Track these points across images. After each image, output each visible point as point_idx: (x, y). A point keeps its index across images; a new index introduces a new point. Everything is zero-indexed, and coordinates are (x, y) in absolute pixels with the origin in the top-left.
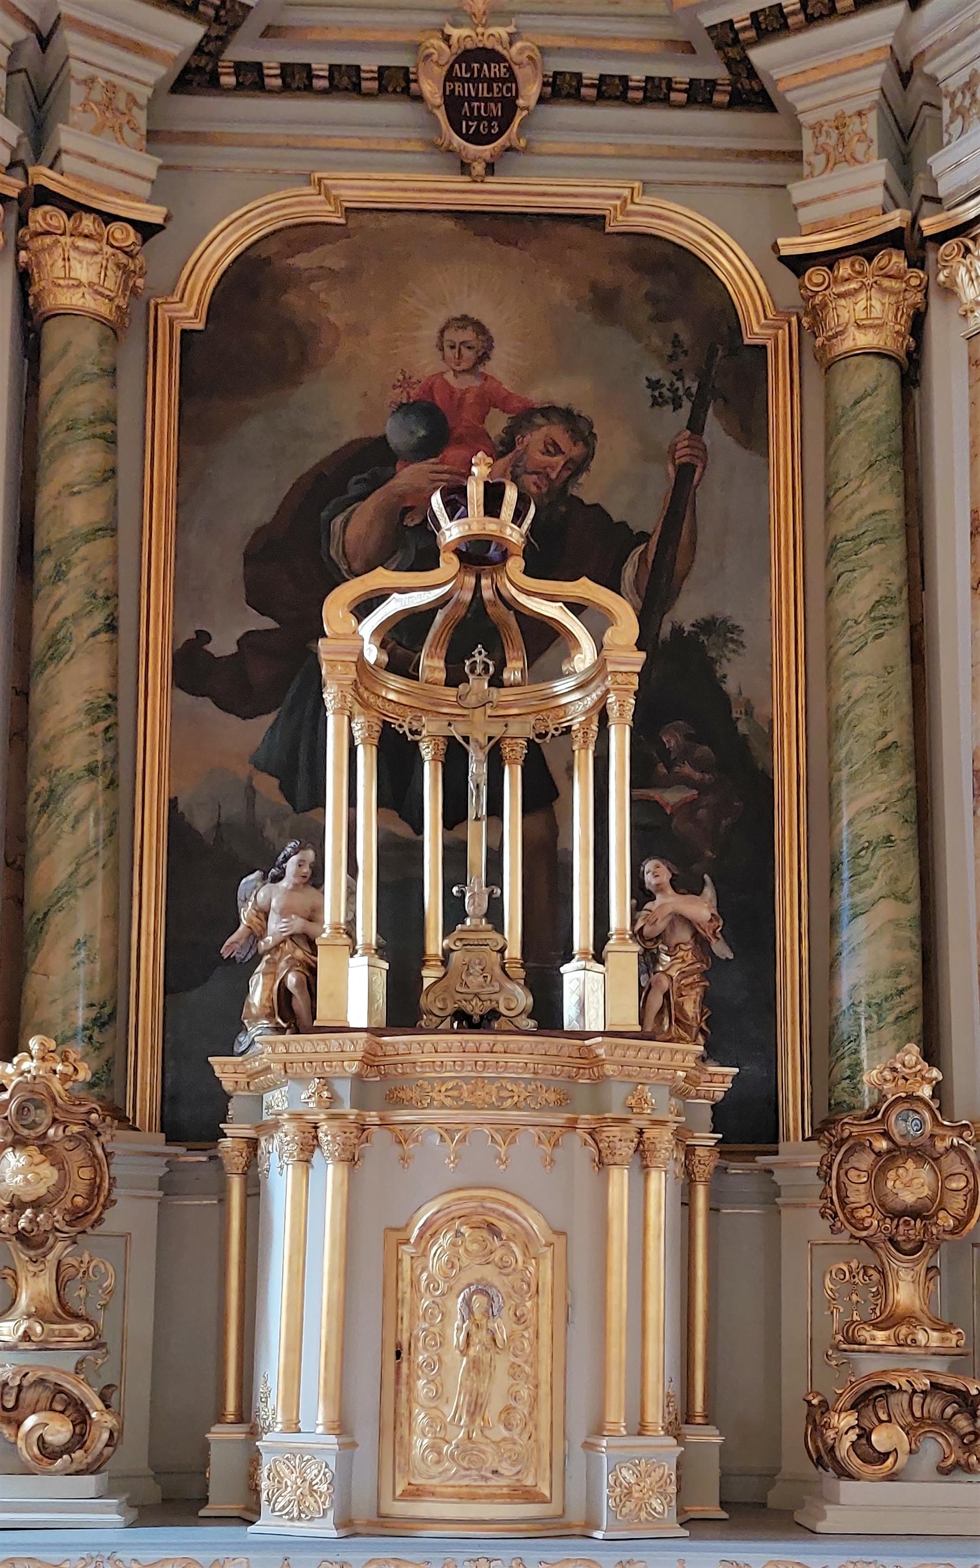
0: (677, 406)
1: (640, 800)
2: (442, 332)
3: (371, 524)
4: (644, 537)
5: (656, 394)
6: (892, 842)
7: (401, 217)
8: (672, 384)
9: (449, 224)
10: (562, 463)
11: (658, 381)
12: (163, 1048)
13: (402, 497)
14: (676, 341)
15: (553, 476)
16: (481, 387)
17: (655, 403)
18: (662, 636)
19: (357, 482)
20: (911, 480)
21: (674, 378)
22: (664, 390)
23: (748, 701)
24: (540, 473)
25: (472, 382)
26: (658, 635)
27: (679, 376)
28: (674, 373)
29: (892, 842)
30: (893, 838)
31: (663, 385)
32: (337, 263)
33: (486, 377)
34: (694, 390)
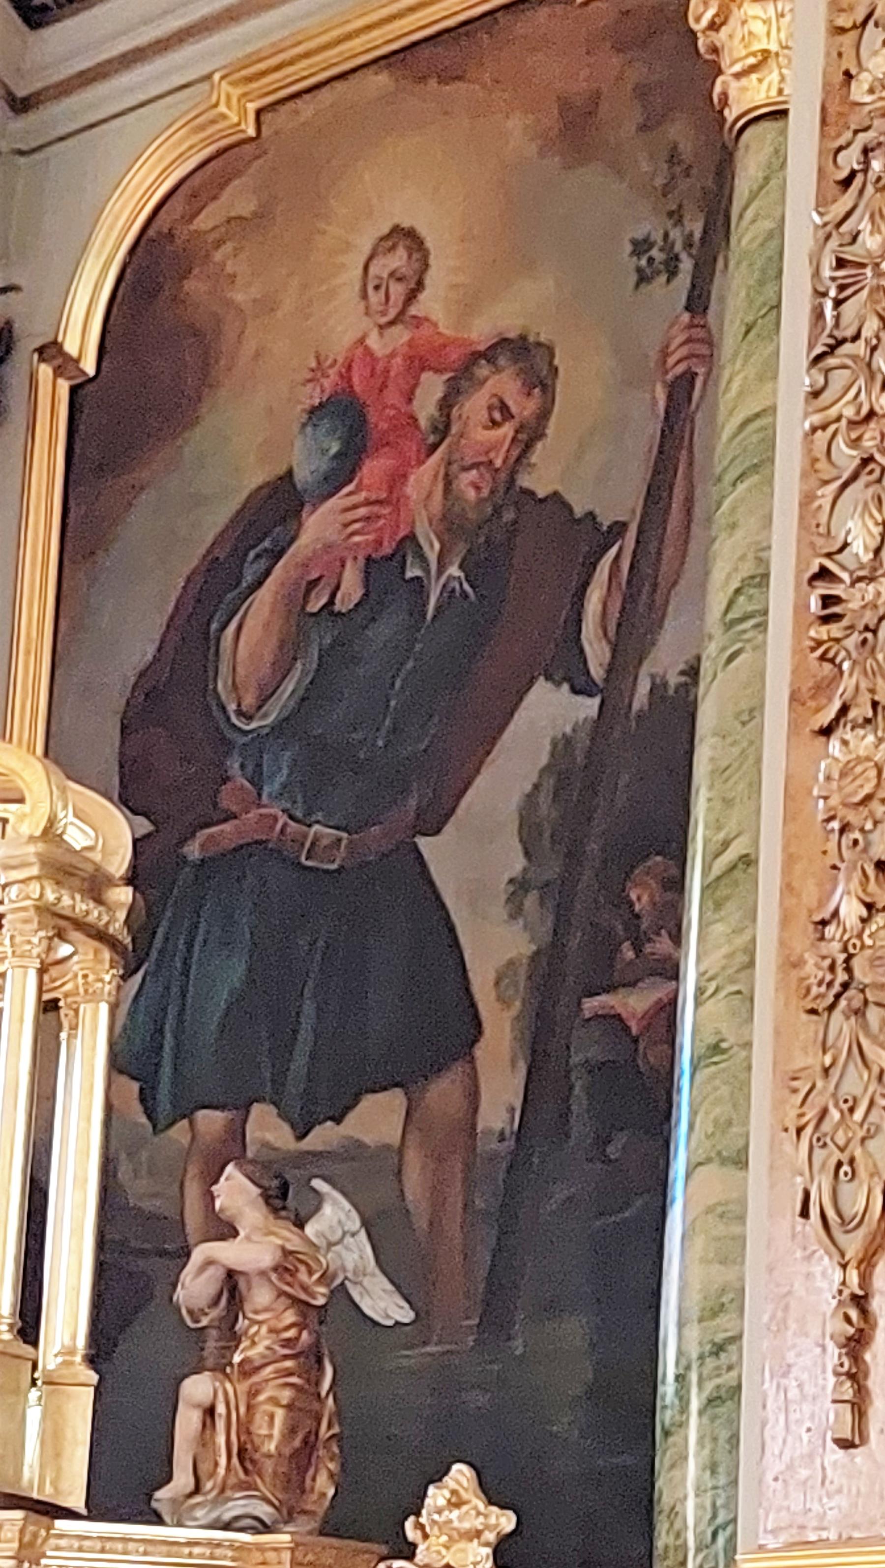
0: (672, 268)
1: (597, 1016)
2: (366, 268)
3: (267, 625)
4: (619, 529)
5: (643, 262)
6: (724, 1051)
7: (325, 94)
8: (666, 235)
9: (381, 80)
10: (511, 434)
11: (646, 240)
12: (415, 44)
13: (305, 566)
14: (673, 158)
15: (498, 463)
16: (410, 344)
17: (643, 278)
18: (636, 706)
19: (258, 556)
20: (37, 1196)
21: (669, 223)
22: (655, 252)
23: (513, 917)
24: (481, 463)
25: (400, 335)
26: (630, 706)
27: (676, 216)
28: (671, 214)
29: (724, 1051)
30: (724, 1045)
31: (651, 245)
32: (246, 207)
33: (418, 322)
34: (697, 235)
